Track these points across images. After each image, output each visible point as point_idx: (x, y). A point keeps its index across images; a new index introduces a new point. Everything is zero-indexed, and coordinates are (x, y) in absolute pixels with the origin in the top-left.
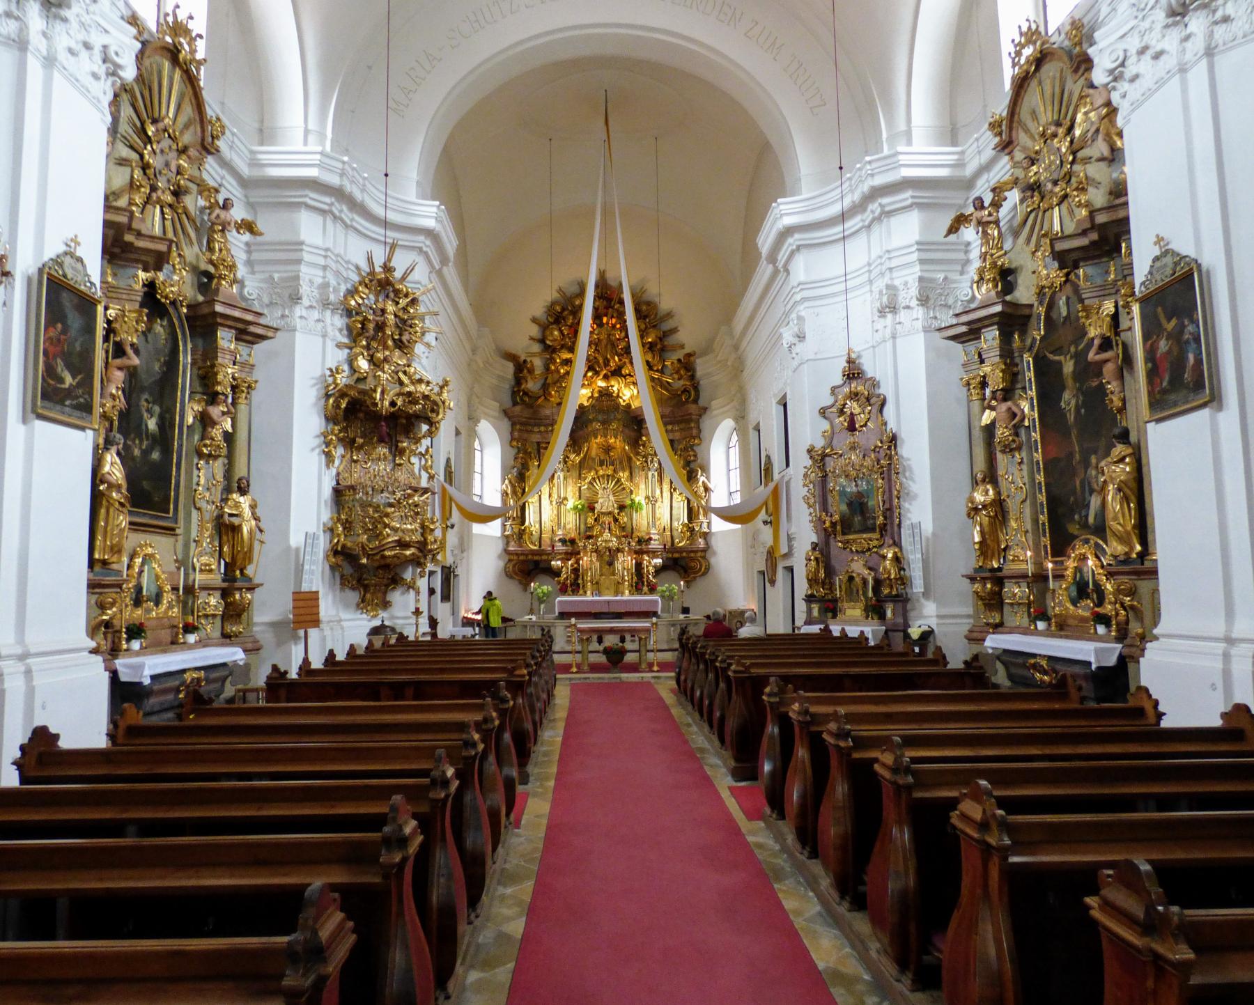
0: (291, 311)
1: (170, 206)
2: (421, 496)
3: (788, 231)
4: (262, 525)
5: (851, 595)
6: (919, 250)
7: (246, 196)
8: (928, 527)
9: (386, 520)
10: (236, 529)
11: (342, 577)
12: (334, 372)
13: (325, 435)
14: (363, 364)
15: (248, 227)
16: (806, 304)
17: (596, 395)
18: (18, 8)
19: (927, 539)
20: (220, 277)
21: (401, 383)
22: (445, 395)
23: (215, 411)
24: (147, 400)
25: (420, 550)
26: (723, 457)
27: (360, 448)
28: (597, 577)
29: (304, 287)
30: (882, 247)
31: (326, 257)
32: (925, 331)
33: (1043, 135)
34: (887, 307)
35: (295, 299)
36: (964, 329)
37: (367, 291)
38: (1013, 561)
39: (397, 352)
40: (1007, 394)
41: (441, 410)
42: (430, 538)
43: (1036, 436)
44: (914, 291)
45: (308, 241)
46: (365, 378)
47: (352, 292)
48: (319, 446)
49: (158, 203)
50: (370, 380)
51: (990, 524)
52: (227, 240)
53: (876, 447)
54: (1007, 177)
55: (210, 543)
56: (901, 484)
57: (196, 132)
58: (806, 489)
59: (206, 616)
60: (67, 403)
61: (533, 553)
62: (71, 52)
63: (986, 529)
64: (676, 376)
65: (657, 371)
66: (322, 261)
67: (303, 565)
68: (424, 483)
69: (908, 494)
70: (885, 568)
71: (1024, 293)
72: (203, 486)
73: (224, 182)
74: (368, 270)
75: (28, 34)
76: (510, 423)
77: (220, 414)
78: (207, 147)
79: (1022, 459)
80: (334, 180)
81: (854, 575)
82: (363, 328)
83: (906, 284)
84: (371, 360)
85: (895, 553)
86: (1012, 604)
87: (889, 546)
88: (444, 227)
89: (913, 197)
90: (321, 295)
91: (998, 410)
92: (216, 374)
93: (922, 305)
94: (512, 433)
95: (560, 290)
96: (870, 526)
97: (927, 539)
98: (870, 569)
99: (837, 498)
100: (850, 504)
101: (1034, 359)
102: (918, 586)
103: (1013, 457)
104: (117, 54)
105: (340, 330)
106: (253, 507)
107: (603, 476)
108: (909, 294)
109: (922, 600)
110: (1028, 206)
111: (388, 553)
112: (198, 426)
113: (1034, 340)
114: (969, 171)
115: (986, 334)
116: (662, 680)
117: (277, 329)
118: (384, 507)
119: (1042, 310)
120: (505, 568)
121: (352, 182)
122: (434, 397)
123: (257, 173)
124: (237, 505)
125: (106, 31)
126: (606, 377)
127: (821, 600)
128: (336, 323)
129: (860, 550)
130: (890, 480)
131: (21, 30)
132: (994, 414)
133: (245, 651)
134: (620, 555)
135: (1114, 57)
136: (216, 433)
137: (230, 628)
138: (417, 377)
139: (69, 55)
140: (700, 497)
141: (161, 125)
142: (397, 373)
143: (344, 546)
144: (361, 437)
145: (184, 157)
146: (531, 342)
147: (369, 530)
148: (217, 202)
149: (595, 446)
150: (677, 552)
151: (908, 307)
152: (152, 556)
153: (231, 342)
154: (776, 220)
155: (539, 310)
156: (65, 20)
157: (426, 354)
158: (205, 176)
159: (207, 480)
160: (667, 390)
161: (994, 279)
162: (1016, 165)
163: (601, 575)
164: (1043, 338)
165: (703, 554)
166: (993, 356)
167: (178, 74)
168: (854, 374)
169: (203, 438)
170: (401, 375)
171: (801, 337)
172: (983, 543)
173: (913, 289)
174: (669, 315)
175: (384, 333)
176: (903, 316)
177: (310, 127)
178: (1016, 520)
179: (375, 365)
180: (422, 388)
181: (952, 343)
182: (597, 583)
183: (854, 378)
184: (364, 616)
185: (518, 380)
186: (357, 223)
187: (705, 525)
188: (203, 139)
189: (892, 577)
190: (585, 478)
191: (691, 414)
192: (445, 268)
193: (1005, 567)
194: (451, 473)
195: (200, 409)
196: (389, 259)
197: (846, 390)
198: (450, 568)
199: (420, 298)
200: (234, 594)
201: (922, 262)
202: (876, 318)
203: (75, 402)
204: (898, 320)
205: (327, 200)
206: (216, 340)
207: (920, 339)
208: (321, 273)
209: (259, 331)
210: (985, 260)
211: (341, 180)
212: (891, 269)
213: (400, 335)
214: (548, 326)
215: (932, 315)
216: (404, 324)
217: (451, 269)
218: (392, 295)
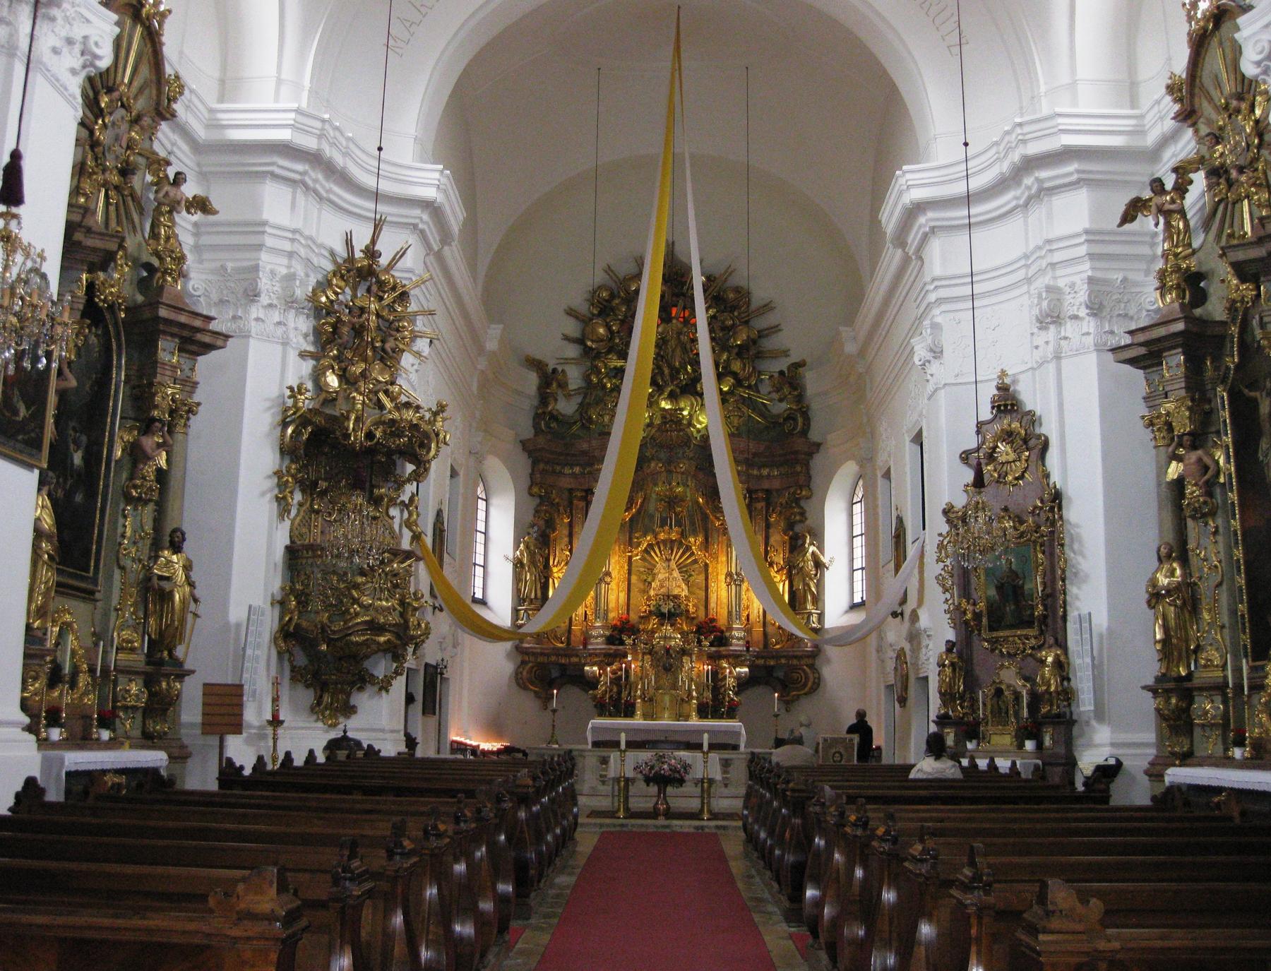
0: (247, 312)
1: (116, 188)
2: (402, 562)
3: (919, 208)
4: (197, 593)
5: (1000, 715)
6: (1087, 241)
7: (199, 165)
8: (1101, 620)
9: (355, 593)
10: (166, 597)
11: (293, 669)
12: (295, 392)
13: (278, 474)
14: (332, 381)
15: (201, 205)
16: (944, 307)
17: (657, 422)
18: (10, 11)
19: (1101, 636)
20: (165, 272)
21: (381, 406)
22: (439, 424)
23: (149, 442)
24: (74, 429)
25: (398, 636)
26: (843, 517)
27: (323, 493)
28: (652, 691)
29: (264, 280)
30: (1027, 240)
31: (292, 240)
32: (1098, 351)
33: (1226, 108)
34: (1048, 315)
35: (252, 295)
36: (1142, 351)
37: (342, 284)
38: (1205, 666)
39: (377, 366)
40: (1198, 439)
41: (433, 445)
42: (412, 621)
43: (1233, 496)
44: (1083, 295)
45: (272, 220)
46: (335, 400)
47: (323, 285)
48: (271, 490)
49: (103, 186)
50: (340, 401)
51: (1177, 617)
52: (174, 223)
53: (1036, 507)
54: (1192, 155)
55: (133, 613)
56: (1066, 561)
57: (150, 98)
58: (942, 565)
59: (126, 708)
60: (20, 437)
61: (557, 652)
62: (55, 51)
63: (1172, 623)
64: (776, 396)
65: (749, 387)
66: (287, 246)
67: (244, 649)
68: (406, 544)
69: (1076, 574)
70: (1043, 677)
71: (1215, 309)
72: (129, 539)
73: (175, 149)
74: (345, 255)
75: (18, 40)
76: (530, 461)
77: (154, 446)
78: (163, 112)
79: (1217, 528)
80: (310, 143)
81: (1003, 687)
82: (334, 333)
83: (1072, 285)
84: (343, 377)
85: (1057, 658)
86: (1203, 726)
87: (1050, 647)
88: (447, 197)
89: (1078, 171)
90: (283, 289)
91: (1187, 462)
92: (155, 395)
93: (1094, 315)
94: (532, 475)
95: (609, 270)
96: (1026, 618)
97: (1101, 636)
98: (1026, 679)
99: (983, 577)
100: (1000, 588)
101: (1228, 393)
102: (1085, 703)
103: (1206, 524)
104: (96, 44)
105: (306, 336)
106: (188, 568)
107: (664, 542)
108: (1076, 301)
109: (1094, 723)
110: (1215, 195)
111: (355, 639)
112: (127, 465)
113: (1228, 368)
114: (1151, 139)
115: (1169, 359)
116: (730, 832)
117: (227, 337)
118: (353, 575)
119: (1234, 330)
120: (517, 674)
121: (333, 145)
122: (424, 427)
123: (215, 136)
124: (169, 562)
125: (88, 21)
126: (672, 397)
127: (957, 723)
128: (300, 327)
129: (1012, 652)
130: (1052, 554)
131: (11, 35)
132: (1181, 466)
133: (170, 757)
134: (686, 659)
135: (1259, 48)
136: (149, 470)
137: (151, 726)
138: (403, 399)
139: (52, 55)
140: (808, 575)
141: (116, 95)
142: (376, 393)
143: (297, 626)
144: (325, 480)
145: (137, 128)
146: (566, 342)
147: (331, 605)
148: (167, 177)
149: (654, 496)
150: (773, 657)
151: (1075, 317)
152: (69, 625)
153: (173, 354)
154: (901, 193)
155: (579, 301)
156: (53, 19)
157: (415, 367)
158: (157, 147)
159: (134, 531)
160: (761, 415)
161: (1178, 287)
162: (1200, 141)
163: (657, 689)
164: (1238, 367)
165: (810, 661)
166: (1178, 388)
167: (139, 29)
168: (1006, 406)
169: (131, 478)
170: (382, 396)
171: (937, 352)
172: (1166, 642)
173: (1082, 293)
174: (767, 307)
175: (362, 339)
176: (1069, 329)
177: (283, 76)
178: (1209, 611)
179: (348, 382)
180: (409, 415)
181: (1127, 367)
182: (651, 700)
183: (1006, 411)
184: (320, 724)
185: (544, 397)
186: (335, 194)
187: (814, 618)
188: (158, 103)
189: (1053, 689)
190: (639, 544)
191: (797, 452)
192: (446, 248)
193: (1196, 675)
194: (442, 531)
195: (131, 440)
196: (373, 242)
197: (997, 427)
198: (436, 667)
199: (412, 292)
200: (160, 683)
201: (1092, 256)
202: (1036, 330)
203: (26, 437)
204: (1063, 334)
205: (300, 167)
206: (156, 352)
207: (1092, 360)
208: (285, 261)
209: (207, 339)
210: (1167, 261)
211: (319, 143)
212: (1053, 265)
213: (383, 341)
214: (591, 320)
215: (1107, 329)
216: (390, 327)
217: (455, 249)
218: (374, 288)
